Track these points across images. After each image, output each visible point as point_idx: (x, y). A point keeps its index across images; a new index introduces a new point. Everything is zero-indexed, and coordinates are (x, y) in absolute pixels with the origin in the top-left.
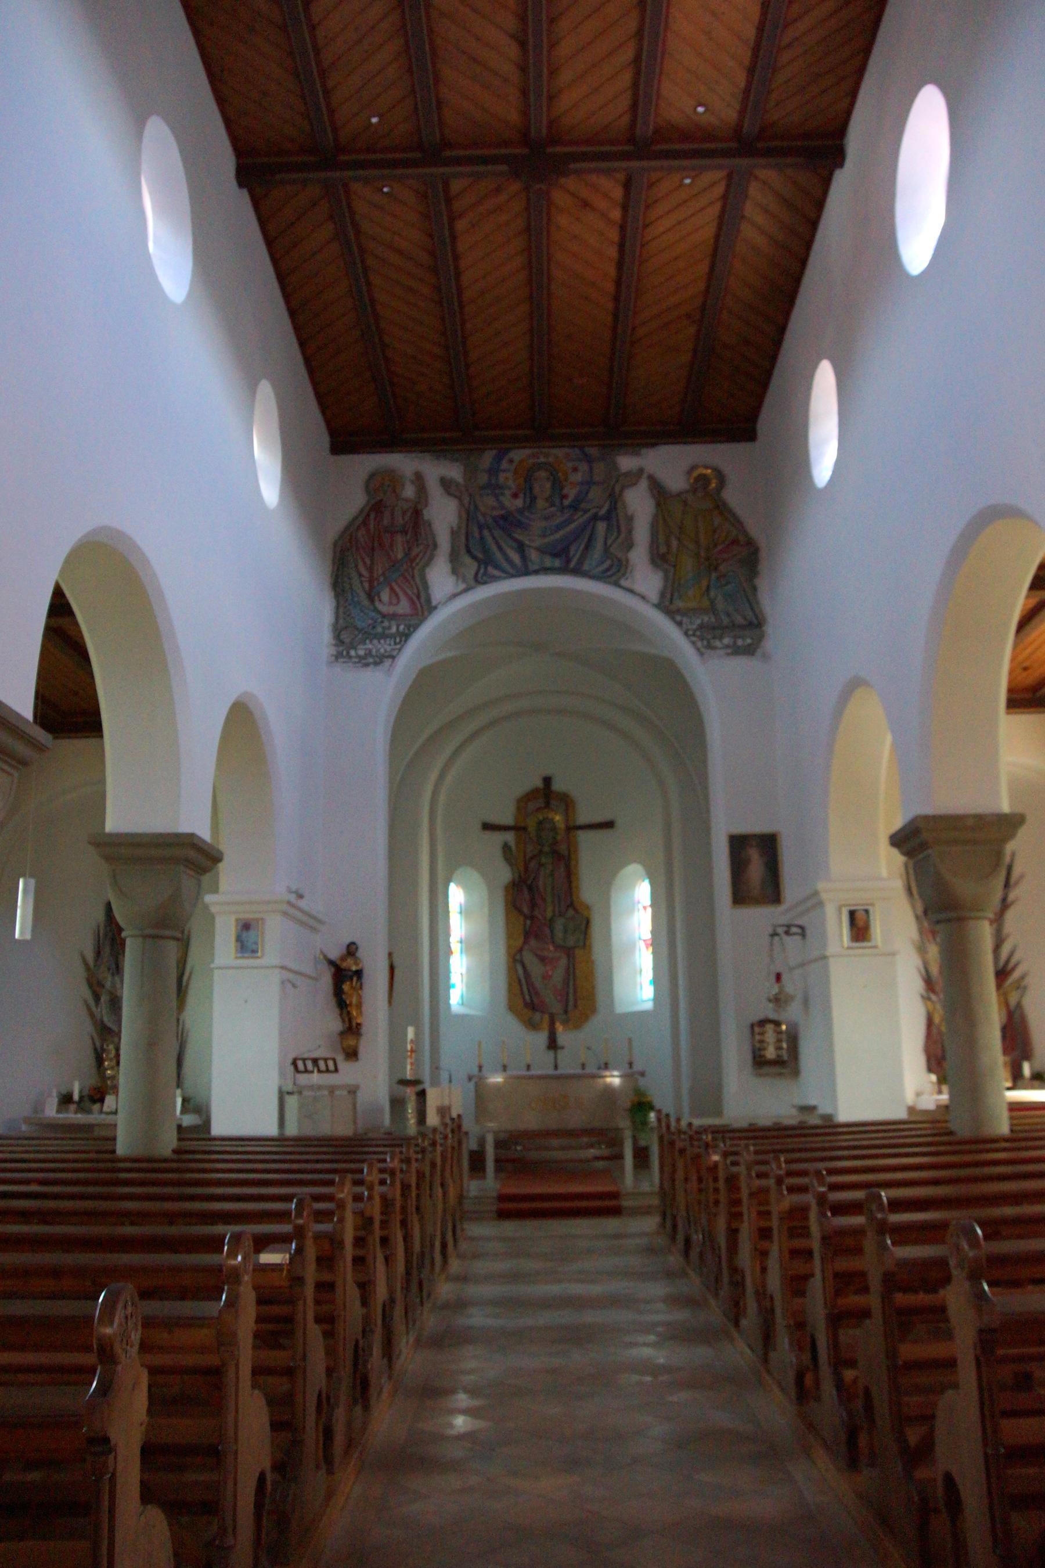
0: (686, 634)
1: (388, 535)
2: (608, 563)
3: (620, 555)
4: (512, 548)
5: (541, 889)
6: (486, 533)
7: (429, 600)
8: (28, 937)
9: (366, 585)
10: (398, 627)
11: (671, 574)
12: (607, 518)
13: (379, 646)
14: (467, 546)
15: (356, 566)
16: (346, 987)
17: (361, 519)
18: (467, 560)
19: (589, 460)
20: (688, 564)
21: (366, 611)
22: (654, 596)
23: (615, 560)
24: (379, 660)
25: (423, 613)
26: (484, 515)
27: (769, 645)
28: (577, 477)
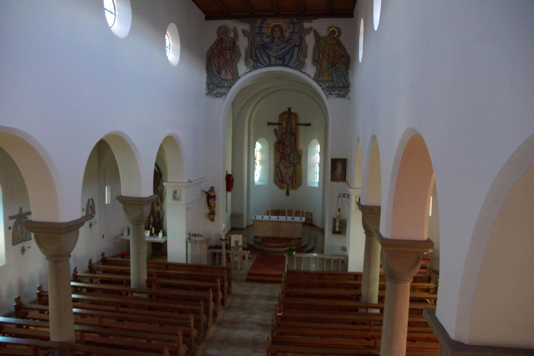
0: (323, 89)
1: (224, 51)
2: (298, 63)
3: (302, 59)
4: (266, 57)
6: (257, 50)
7: (238, 74)
9: (217, 68)
12: (299, 46)
13: (222, 90)
14: (251, 55)
15: (214, 62)
17: (215, 45)
18: (250, 60)
19: (293, 23)
20: (325, 63)
21: (217, 78)
22: (313, 75)
23: (300, 62)
25: (236, 79)
26: (257, 44)
27: (350, 94)
28: (289, 30)
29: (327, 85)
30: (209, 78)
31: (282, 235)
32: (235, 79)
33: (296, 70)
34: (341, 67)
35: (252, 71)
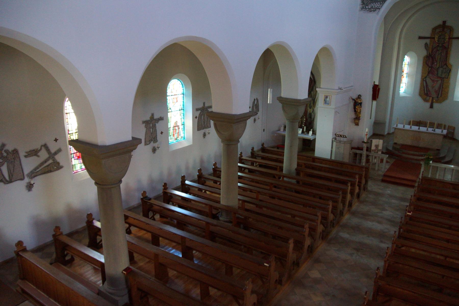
8: (271, 103)
13: (375, 5)
31: (421, 145)
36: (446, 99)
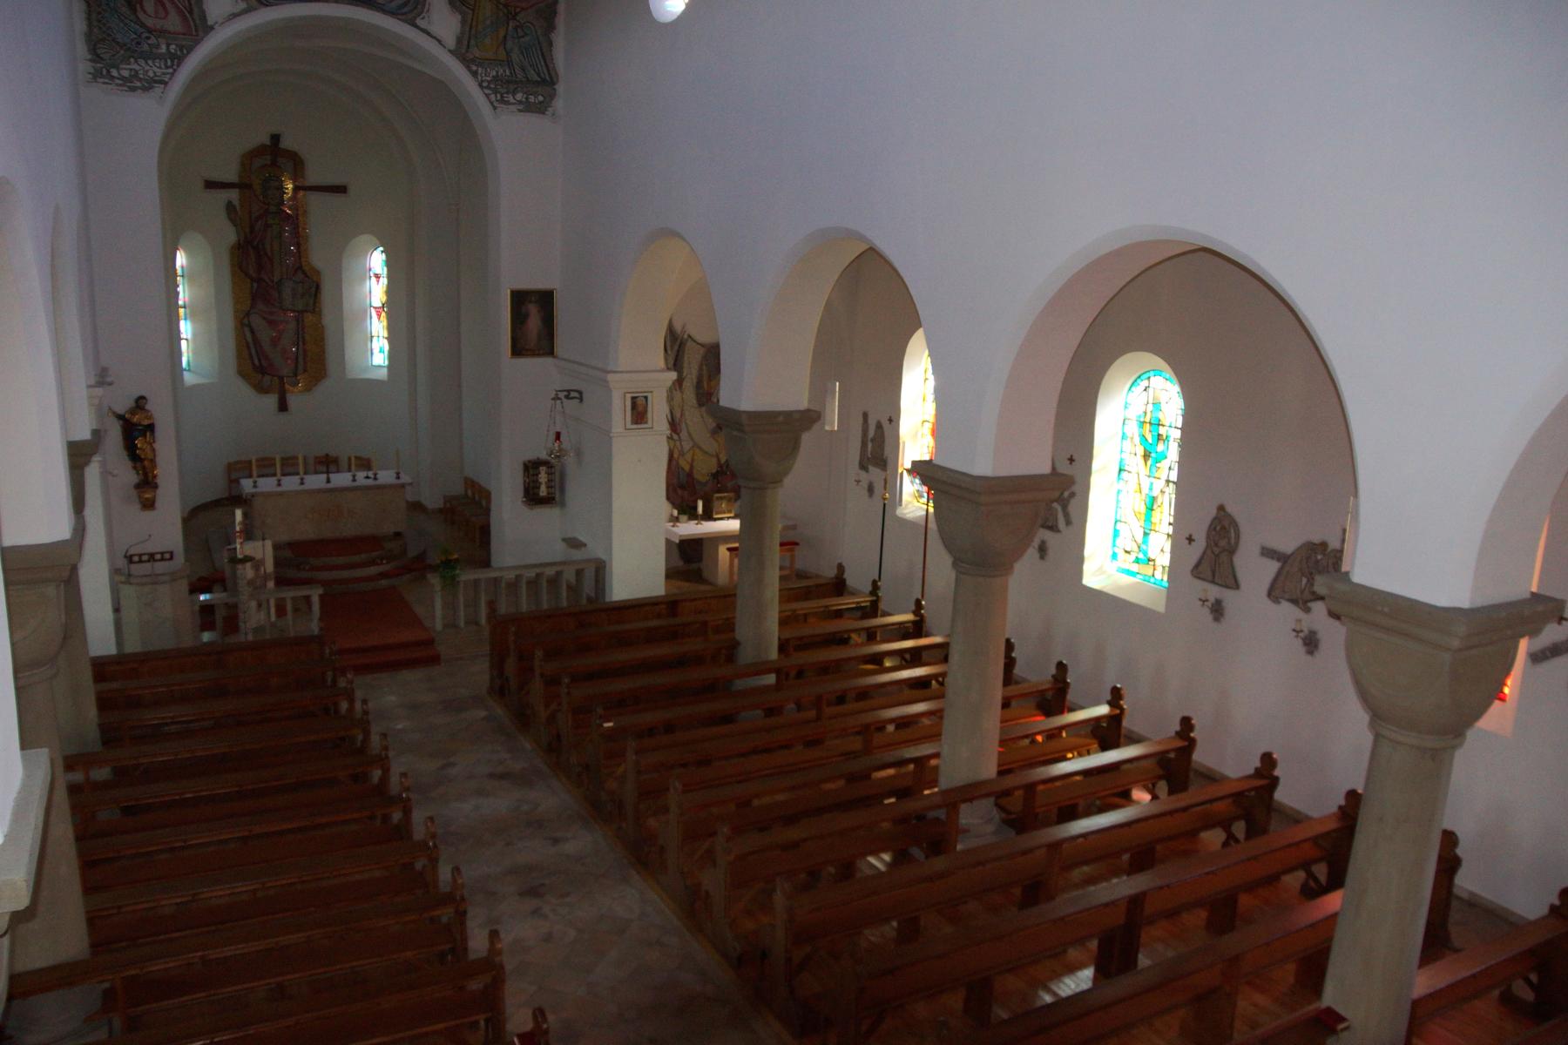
0: (480, 86)
5: (269, 254)
7: (204, 17)
10: (168, 45)
11: (470, 16)
16: (139, 443)
22: (451, 42)
24: (149, 85)
29: (494, 73)
30: (94, 16)
31: (348, 529)
32: (194, 33)
33: (400, 20)
34: (532, 24)
35: (256, 9)
36: (323, 378)
